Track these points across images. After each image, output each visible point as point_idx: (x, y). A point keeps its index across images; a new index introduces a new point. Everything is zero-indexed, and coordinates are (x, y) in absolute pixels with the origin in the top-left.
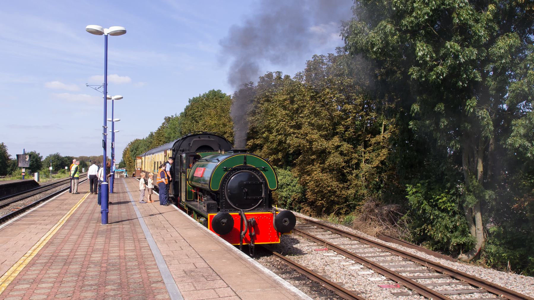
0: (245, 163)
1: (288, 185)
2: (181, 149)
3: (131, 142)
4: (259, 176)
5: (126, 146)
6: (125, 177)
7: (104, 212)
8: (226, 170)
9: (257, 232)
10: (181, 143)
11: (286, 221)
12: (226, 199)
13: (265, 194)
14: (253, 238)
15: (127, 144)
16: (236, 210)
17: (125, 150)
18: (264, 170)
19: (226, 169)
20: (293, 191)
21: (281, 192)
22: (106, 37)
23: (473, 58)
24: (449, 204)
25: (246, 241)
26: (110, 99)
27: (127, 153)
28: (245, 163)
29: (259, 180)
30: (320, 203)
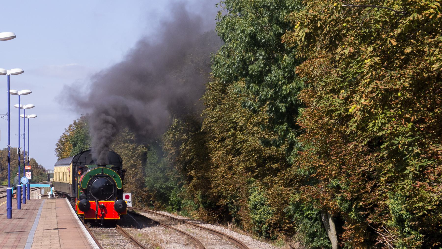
0: (103, 173)
1: (263, 204)
2: (79, 161)
3: (75, 123)
4: (111, 181)
5: (64, 131)
6: (50, 197)
7: (9, 210)
8: (91, 176)
9: (106, 212)
10: (80, 156)
11: (121, 206)
12: (90, 194)
13: (114, 191)
14: (104, 216)
15: (67, 126)
16: (94, 199)
17: (61, 141)
18: (114, 177)
19: (91, 176)
20: (268, 213)
21: (254, 214)
22: (20, 96)
23: (282, 111)
24: (309, 212)
25: (100, 217)
26: (22, 108)
27: (67, 149)
28: (103, 173)
29: (110, 183)
30: (288, 227)
